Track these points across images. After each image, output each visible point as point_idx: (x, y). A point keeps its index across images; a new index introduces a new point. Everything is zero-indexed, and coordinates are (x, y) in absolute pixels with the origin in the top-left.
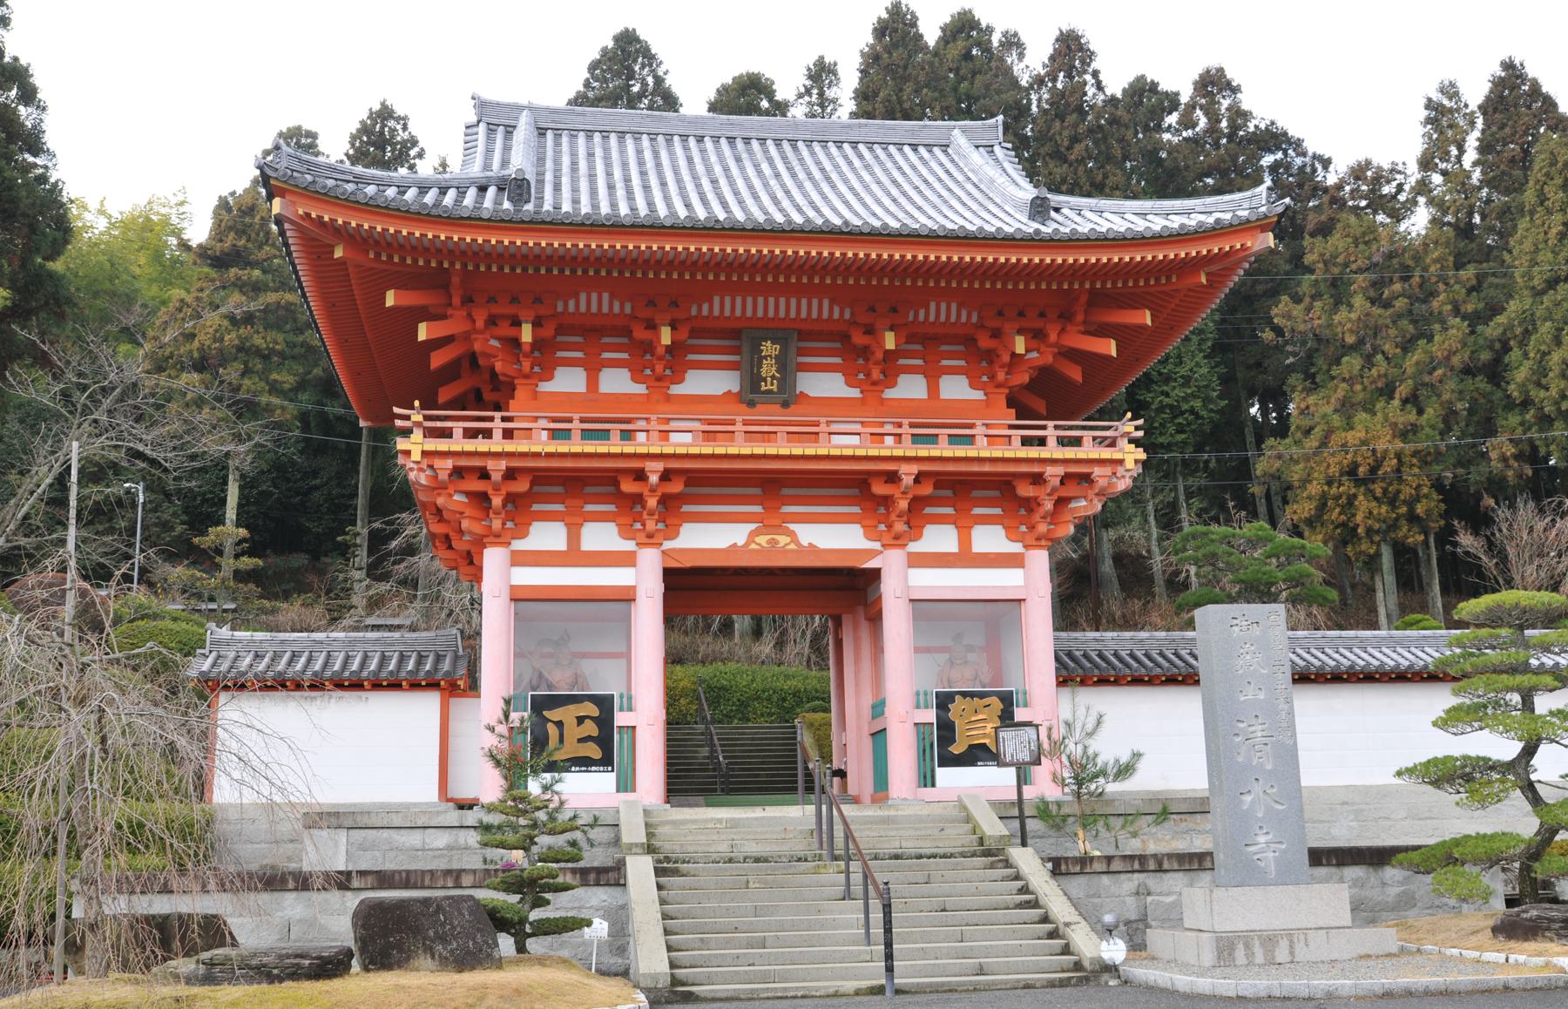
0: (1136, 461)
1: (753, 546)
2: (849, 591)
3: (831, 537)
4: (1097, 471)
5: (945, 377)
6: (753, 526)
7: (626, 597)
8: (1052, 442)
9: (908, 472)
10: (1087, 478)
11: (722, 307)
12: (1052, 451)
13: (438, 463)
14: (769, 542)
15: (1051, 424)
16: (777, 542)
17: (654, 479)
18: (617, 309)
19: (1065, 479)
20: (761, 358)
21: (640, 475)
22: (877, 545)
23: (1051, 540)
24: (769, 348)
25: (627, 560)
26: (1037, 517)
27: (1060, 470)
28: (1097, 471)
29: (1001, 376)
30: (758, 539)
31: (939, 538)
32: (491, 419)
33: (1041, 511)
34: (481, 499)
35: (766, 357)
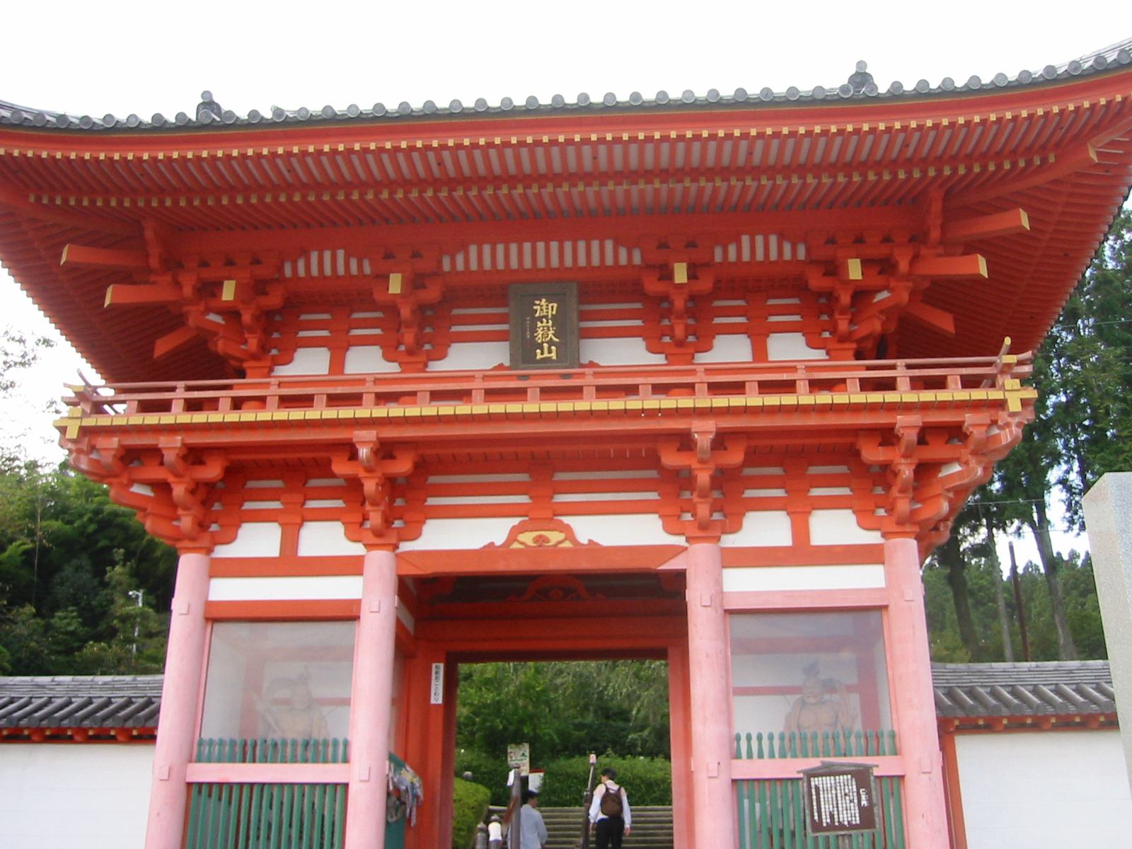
0: (1024, 403)
1: (516, 546)
2: (643, 608)
3: (618, 531)
4: (969, 418)
5: (774, 336)
6: (515, 521)
7: (347, 614)
8: (903, 384)
9: (703, 432)
10: (955, 432)
11: (480, 258)
12: (904, 394)
13: (102, 442)
14: (536, 540)
15: (900, 363)
16: (547, 540)
17: (364, 452)
18: (354, 269)
19: (926, 434)
20: (535, 320)
21: (350, 450)
22: (680, 541)
23: (919, 524)
24: (545, 308)
25: (351, 566)
26: (895, 492)
27: (916, 419)
28: (969, 418)
29: (843, 325)
30: (522, 537)
31: (766, 528)
32: (173, 389)
33: (899, 483)
34: (162, 488)
35: (540, 319)
